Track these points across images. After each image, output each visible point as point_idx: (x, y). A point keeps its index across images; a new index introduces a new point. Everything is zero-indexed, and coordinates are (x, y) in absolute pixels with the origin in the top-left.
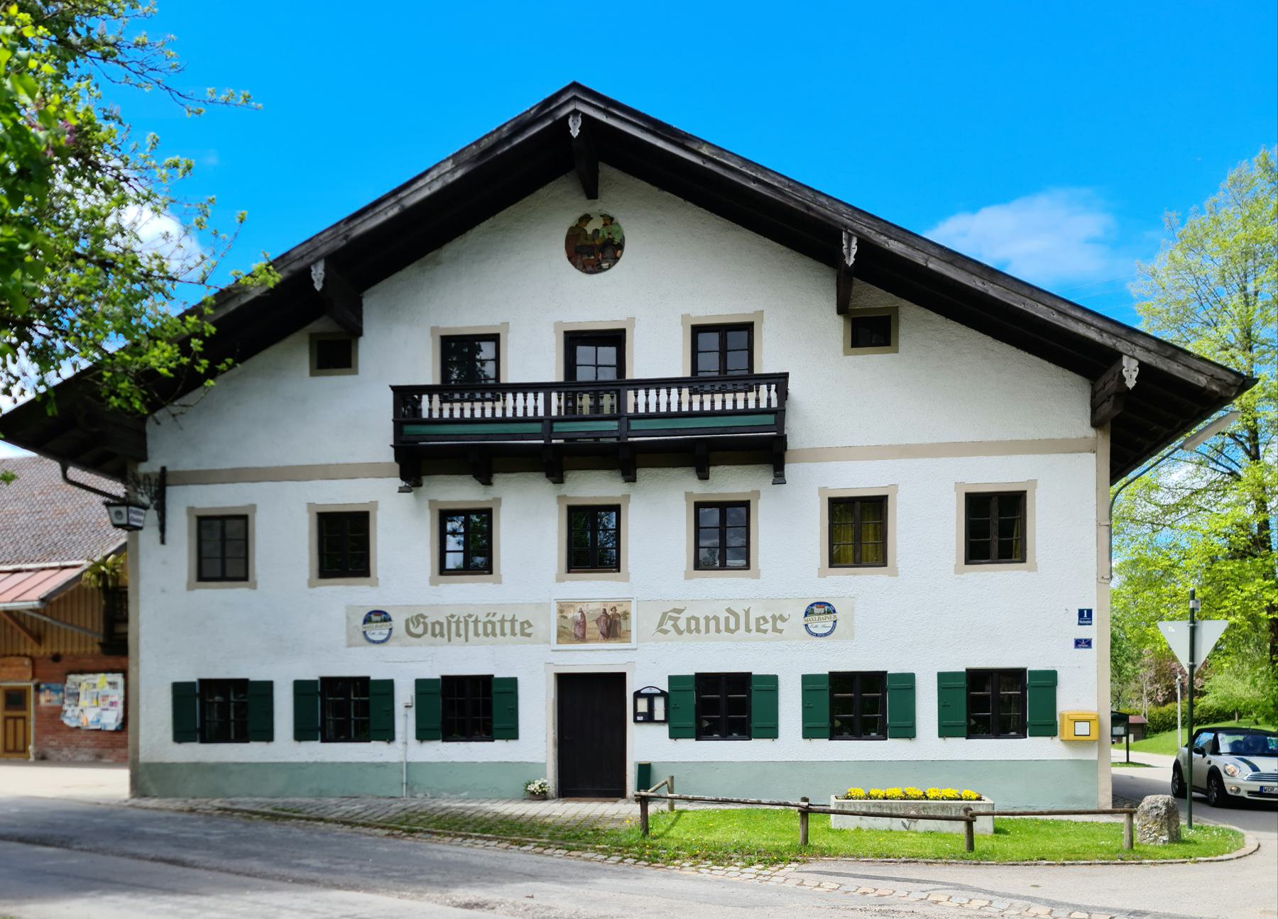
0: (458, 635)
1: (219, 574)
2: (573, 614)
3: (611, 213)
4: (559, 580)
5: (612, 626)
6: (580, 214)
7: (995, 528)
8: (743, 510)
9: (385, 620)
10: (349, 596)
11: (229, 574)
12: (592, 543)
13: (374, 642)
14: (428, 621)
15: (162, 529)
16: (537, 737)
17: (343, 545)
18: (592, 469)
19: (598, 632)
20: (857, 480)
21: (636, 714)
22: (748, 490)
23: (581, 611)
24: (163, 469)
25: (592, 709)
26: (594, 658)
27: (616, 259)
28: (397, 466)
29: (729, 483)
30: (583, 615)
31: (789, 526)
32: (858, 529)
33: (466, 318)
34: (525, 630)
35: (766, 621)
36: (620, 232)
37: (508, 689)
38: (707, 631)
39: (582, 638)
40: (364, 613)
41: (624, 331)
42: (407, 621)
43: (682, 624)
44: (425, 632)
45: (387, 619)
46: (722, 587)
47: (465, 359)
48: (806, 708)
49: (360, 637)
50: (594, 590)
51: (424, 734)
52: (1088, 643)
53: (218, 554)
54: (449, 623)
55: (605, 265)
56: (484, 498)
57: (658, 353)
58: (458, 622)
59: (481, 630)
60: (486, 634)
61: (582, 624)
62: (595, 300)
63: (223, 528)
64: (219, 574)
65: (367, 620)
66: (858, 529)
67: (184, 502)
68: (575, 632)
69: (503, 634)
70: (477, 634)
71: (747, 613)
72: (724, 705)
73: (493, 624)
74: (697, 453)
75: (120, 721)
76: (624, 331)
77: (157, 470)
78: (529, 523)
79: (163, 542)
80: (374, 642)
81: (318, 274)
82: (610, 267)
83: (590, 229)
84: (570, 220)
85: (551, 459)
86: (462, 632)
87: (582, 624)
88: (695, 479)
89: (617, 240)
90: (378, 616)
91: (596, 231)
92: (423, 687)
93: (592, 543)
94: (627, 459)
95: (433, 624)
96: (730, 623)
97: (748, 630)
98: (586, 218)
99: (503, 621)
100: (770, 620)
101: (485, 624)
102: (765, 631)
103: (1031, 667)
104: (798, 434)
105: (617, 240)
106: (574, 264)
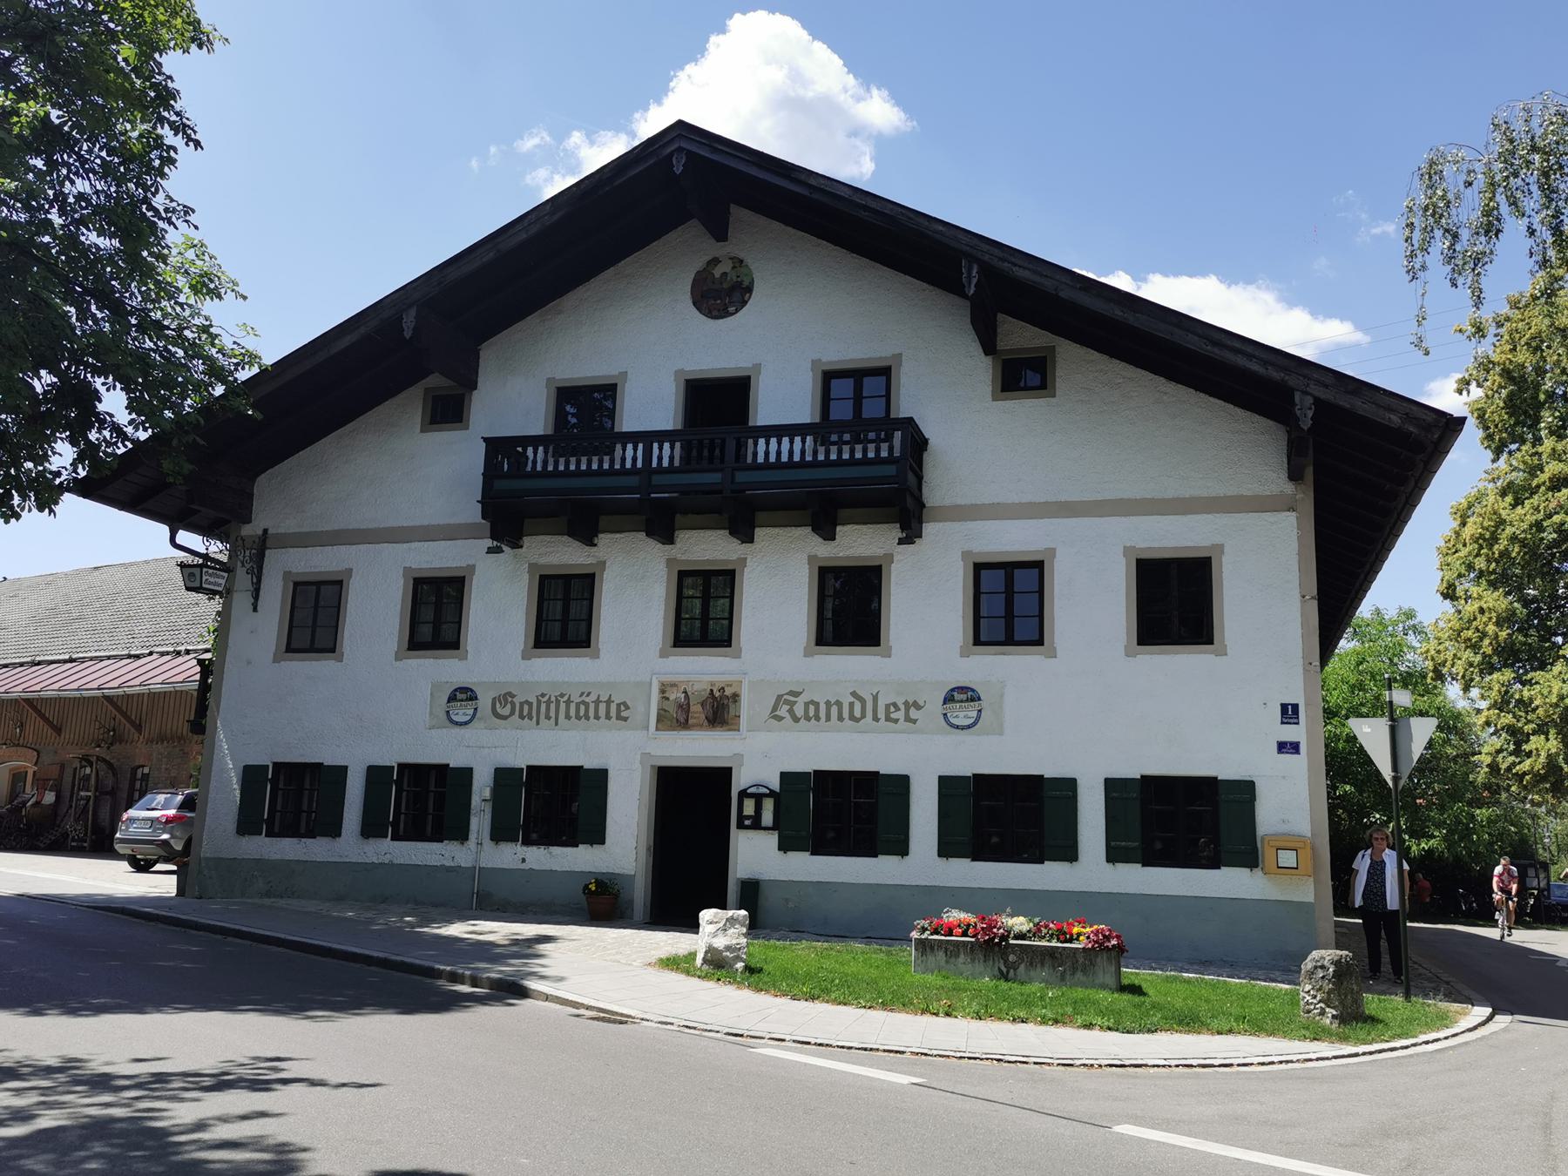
3: (741, 255)
6: (709, 258)
10: (443, 670)
15: (256, 597)
17: (436, 614)
21: (741, 817)
22: (735, 557)
24: (265, 531)
26: (697, 748)
29: (858, 542)
30: (687, 697)
35: (898, 709)
36: (750, 274)
38: (828, 718)
41: (749, 378)
43: (799, 710)
44: (512, 713)
50: (702, 669)
52: (1294, 748)
54: (539, 702)
55: (732, 309)
56: (581, 561)
58: (548, 703)
59: (572, 712)
62: (717, 348)
67: (282, 565)
69: (597, 717)
70: (568, 717)
71: (875, 698)
73: (587, 705)
76: (749, 378)
83: (717, 272)
84: (699, 263)
86: (552, 714)
87: (685, 708)
89: (746, 283)
90: (463, 694)
91: (725, 274)
95: (522, 704)
98: (715, 261)
99: (597, 702)
100: (902, 707)
101: (578, 705)
102: (896, 721)
105: (746, 283)
106: (694, 304)
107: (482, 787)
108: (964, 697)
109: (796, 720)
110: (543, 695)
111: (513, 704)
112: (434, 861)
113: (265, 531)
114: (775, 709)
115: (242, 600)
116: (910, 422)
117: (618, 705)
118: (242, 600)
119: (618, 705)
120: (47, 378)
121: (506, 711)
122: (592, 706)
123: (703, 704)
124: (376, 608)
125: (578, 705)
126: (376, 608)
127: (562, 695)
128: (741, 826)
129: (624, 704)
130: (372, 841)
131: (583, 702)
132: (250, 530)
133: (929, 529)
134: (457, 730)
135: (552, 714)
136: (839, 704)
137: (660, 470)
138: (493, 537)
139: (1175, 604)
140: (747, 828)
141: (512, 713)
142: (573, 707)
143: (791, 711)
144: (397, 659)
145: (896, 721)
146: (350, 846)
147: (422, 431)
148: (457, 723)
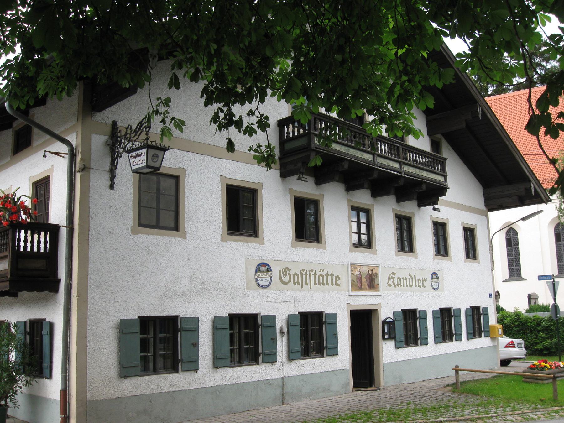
0: (307, 284)
1: (154, 223)
2: (356, 273)
5: (370, 281)
8: (172, 225)
10: (242, 249)
11: (161, 224)
13: (262, 286)
14: (292, 272)
15: (113, 177)
17: (241, 213)
18: (472, 171)
19: (366, 284)
23: (360, 271)
26: (364, 300)
30: (360, 273)
34: (336, 281)
37: (270, 324)
38: (404, 286)
39: (360, 288)
40: (256, 264)
42: (280, 271)
44: (290, 281)
45: (269, 270)
48: (335, 336)
49: (254, 282)
50: (363, 258)
51: (218, 362)
53: (154, 206)
54: (302, 274)
58: (306, 274)
60: (320, 284)
61: (360, 279)
63: (158, 183)
64: (154, 223)
65: (258, 270)
69: (328, 284)
70: (315, 284)
73: (323, 276)
75: (532, 356)
79: (112, 187)
86: (308, 282)
87: (360, 279)
88: (370, 195)
90: (263, 267)
92: (216, 321)
95: (294, 275)
97: (416, 286)
99: (327, 275)
101: (319, 276)
103: (327, 312)
107: (142, 336)
109: (395, 286)
110: (303, 270)
111: (289, 274)
112: (256, 377)
114: (388, 282)
115: (98, 180)
116: (135, 92)
117: (336, 277)
118: (98, 180)
119: (336, 277)
120: (303, 46)
121: (286, 279)
122: (325, 277)
123: (366, 278)
124: (204, 205)
125: (319, 276)
126: (204, 205)
127: (312, 270)
128: (384, 338)
129: (338, 276)
130: (220, 370)
131: (321, 275)
134: (261, 291)
135: (308, 282)
136: (406, 279)
137: (290, 140)
140: (387, 339)
141: (290, 281)
142: (317, 277)
143: (393, 282)
144: (263, 244)
146: (208, 375)
148: (261, 286)
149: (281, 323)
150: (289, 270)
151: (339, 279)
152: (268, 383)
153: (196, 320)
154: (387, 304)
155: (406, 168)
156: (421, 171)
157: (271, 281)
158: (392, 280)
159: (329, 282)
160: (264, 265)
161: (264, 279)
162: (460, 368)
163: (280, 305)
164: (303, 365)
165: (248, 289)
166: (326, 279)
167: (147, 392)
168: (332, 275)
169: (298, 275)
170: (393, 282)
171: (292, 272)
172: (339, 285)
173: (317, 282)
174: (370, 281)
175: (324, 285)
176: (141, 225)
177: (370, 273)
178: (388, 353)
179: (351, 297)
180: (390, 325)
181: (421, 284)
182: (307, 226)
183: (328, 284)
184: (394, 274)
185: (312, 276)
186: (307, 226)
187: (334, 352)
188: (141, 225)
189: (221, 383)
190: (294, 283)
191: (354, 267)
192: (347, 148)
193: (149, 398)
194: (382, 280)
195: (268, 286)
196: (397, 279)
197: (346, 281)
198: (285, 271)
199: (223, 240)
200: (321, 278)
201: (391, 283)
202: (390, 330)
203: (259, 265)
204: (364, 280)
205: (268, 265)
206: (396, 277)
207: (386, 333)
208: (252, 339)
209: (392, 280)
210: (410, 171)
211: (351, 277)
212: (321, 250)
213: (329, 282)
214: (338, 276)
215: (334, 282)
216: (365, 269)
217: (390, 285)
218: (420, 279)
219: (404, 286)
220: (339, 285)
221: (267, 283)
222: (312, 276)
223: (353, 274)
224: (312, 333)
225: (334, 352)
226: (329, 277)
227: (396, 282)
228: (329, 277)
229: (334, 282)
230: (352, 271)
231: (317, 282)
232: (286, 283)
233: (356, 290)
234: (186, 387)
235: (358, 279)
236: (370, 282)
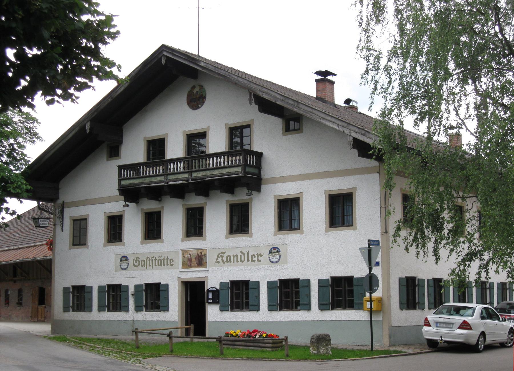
0: (150, 266)
4: (183, 240)
5: (200, 260)
6: (191, 86)
7: (340, 210)
9: (278, 252)
10: (117, 250)
11: (82, 243)
12: (195, 226)
13: (273, 262)
14: (140, 260)
15: (62, 227)
16: (174, 312)
17: (115, 229)
20: (287, 190)
24: (63, 202)
25: (196, 295)
26: (194, 274)
27: (203, 103)
28: (123, 197)
29: (241, 196)
30: (190, 256)
31: (263, 215)
32: (288, 213)
33: (155, 133)
34: (171, 263)
35: (255, 257)
36: (205, 91)
38: (234, 262)
39: (190, 266)
41: (165, 138)
43: (225, 259)
45: (127, 260)
46: (240, 241)
47: (156, 147)
50: (194, 244)
51: (323, 307)
55: (200, 106)
57: (217, 143)
60: (159, 265)
65: (121, 260)
66: (288, 213)
67: (70, 213)
68: (187, 264)
69: (164, 265)
70: (156, 265)
72: (241, 295)
73: (161, 260)
74: (228, 185)
77: (61, 202)
78: (173, 222)
79: (62, 231)
80: (273, 262)
81: (88, 126)
82: (201, 106)
83: (195, 92)
85: (179, 192)
86: (151, 264)
87: (190, 260)
89: (204, 95)
90: (124, 258)
91: (197, 92)
93: (195, 226)
94: (205, 188)
96: (243, 258)
99: (164, 259)
102: (254, 261)
103: (302, 278)
104: (267, 172)
106: (190, 106)
108: (275, 251)
109: (224, 262)
110: (148, 257)
112: (119, 319)
113: (63, 202)
114: (217, 259)
119: (252, 256)
121: (137, 264)
123: (195, 259)
124: (97, 230)
126: (97, 230)
127: (153, 257)
128: (208, 302)
129: (172, 259)
131: (160, 260)
132: (60, 202)
133: (264, 187)
134: (123, 272)
135: (151, 264)
136: (237, 256)
138: (125, 201)
139: (340, 210)
142: (157, 261)
143: (222, 260)
145: (254, 261)
147: (108, 160)
148: (123, 269)
149: (131, 290)
150: (139, 258)
151: (173, 261)
152: (125, 322)
153: (308, 281)
154: (215, 277)
155: (194, 175)
156: (212, 171)
157: (280, 258)
158: (221, 258)
159: (166, 263)
160: (124, 257)
161: (274, 257)
162: (140, 330)
163: (133, 279)
164: (145, 315)
165: (116, 271)
166: (163, 262)
167: (73, 319)
168: (167, 259)
169: (144, 261)
170: (222, 260)
171: (140, 260)
172: (172, 265)
173: (157, 264)
174: (200, 260)
175: (161, 265)
176: (352, 225)
177: (200, 254)
178: (213, 313)
179: (181, 273)
180: (216, 293)
181: (255, 259)
182: (153, 229)
183: (164, 265)
184: (223, 253)
185: (154, 261)
186: (153, 229)
187: (166, 308)
188: (352, 225)
189: (102, 319)
190: (142, 266)
191: (184, 252)
192: (144, 179)
193: (82, 321)
194: (210, 259)
195: (277, 262)
196: (227, 257)
197: (179, 261)
198: (220, 255)
199: (142, 243)
200: (229, 258)
201: (220, 260)
202: (216, 296)
203: (272, 249)
204: (193, 260)
205: (278, 248)
206: (225, 255)
207: (210, 299)
208: (336, 294)
209: (221, 258)
210: (200, 175)
211: (183, 259)
212: (160, 244)
213: (166, 263)
214: (172, 259)
215: (169, 263)
216: (195, 252)
217: (219, 262)
218: (254, 255)
219: (234, 262)
220: (172, 265)
221: (126, 267)
222: (154, 261)
223: (184, 257)
224: (153, 296)
225: (166, 308)
226: (166, 261)
227: (223, 258)
228: (166, 261)
229: (169, 263)
230: (183, 254)
231: (157, 264)
232: (137, 266)
233: (186, 268)
234: (87, 319)
235: (189, 260)
236: (199, 262)
